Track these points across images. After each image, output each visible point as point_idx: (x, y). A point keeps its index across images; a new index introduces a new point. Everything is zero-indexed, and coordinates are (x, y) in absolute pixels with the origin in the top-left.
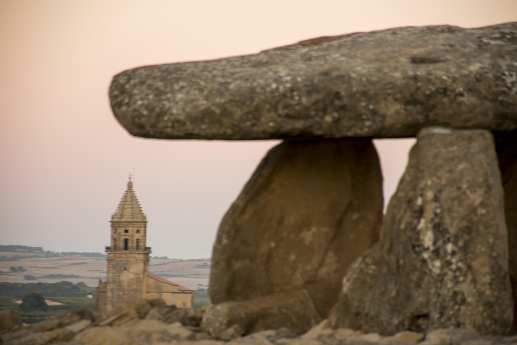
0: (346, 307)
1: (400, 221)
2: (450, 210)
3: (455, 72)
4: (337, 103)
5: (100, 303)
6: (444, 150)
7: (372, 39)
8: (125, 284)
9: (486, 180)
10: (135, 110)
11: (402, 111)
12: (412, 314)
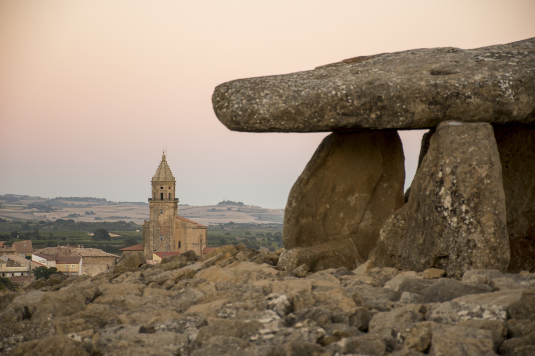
0: (383, 250)
1: (425, 189)
2: (464, 181)
3: (465, 81)
4: (379, 104)
5: (146, 235)
6: (458, 137)
7: (398, 57)
8: (162, 223)
9: (490, 159)
10: (233, 111)
11: (427, 109)
12: (435, 255)
